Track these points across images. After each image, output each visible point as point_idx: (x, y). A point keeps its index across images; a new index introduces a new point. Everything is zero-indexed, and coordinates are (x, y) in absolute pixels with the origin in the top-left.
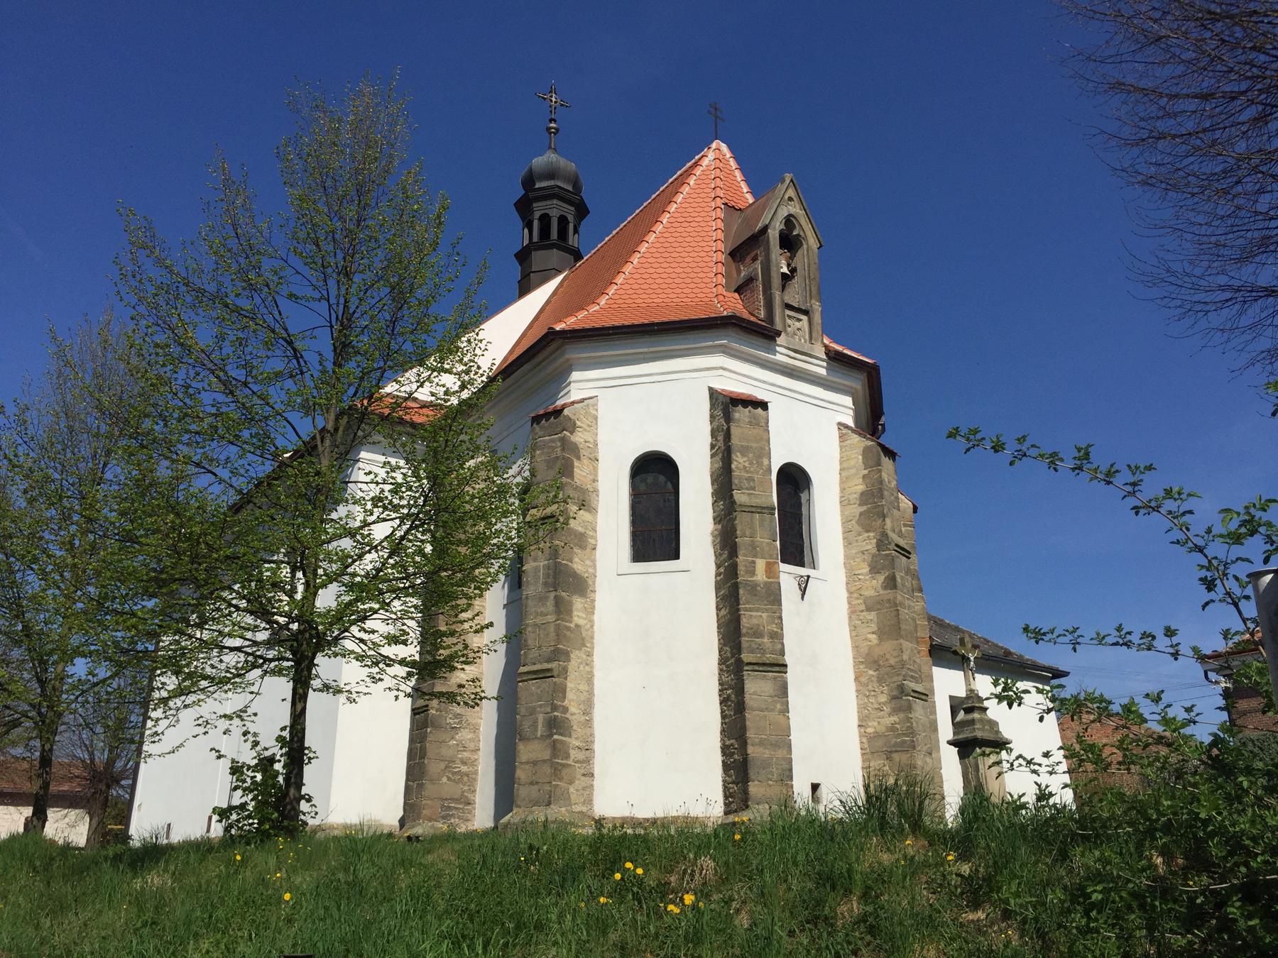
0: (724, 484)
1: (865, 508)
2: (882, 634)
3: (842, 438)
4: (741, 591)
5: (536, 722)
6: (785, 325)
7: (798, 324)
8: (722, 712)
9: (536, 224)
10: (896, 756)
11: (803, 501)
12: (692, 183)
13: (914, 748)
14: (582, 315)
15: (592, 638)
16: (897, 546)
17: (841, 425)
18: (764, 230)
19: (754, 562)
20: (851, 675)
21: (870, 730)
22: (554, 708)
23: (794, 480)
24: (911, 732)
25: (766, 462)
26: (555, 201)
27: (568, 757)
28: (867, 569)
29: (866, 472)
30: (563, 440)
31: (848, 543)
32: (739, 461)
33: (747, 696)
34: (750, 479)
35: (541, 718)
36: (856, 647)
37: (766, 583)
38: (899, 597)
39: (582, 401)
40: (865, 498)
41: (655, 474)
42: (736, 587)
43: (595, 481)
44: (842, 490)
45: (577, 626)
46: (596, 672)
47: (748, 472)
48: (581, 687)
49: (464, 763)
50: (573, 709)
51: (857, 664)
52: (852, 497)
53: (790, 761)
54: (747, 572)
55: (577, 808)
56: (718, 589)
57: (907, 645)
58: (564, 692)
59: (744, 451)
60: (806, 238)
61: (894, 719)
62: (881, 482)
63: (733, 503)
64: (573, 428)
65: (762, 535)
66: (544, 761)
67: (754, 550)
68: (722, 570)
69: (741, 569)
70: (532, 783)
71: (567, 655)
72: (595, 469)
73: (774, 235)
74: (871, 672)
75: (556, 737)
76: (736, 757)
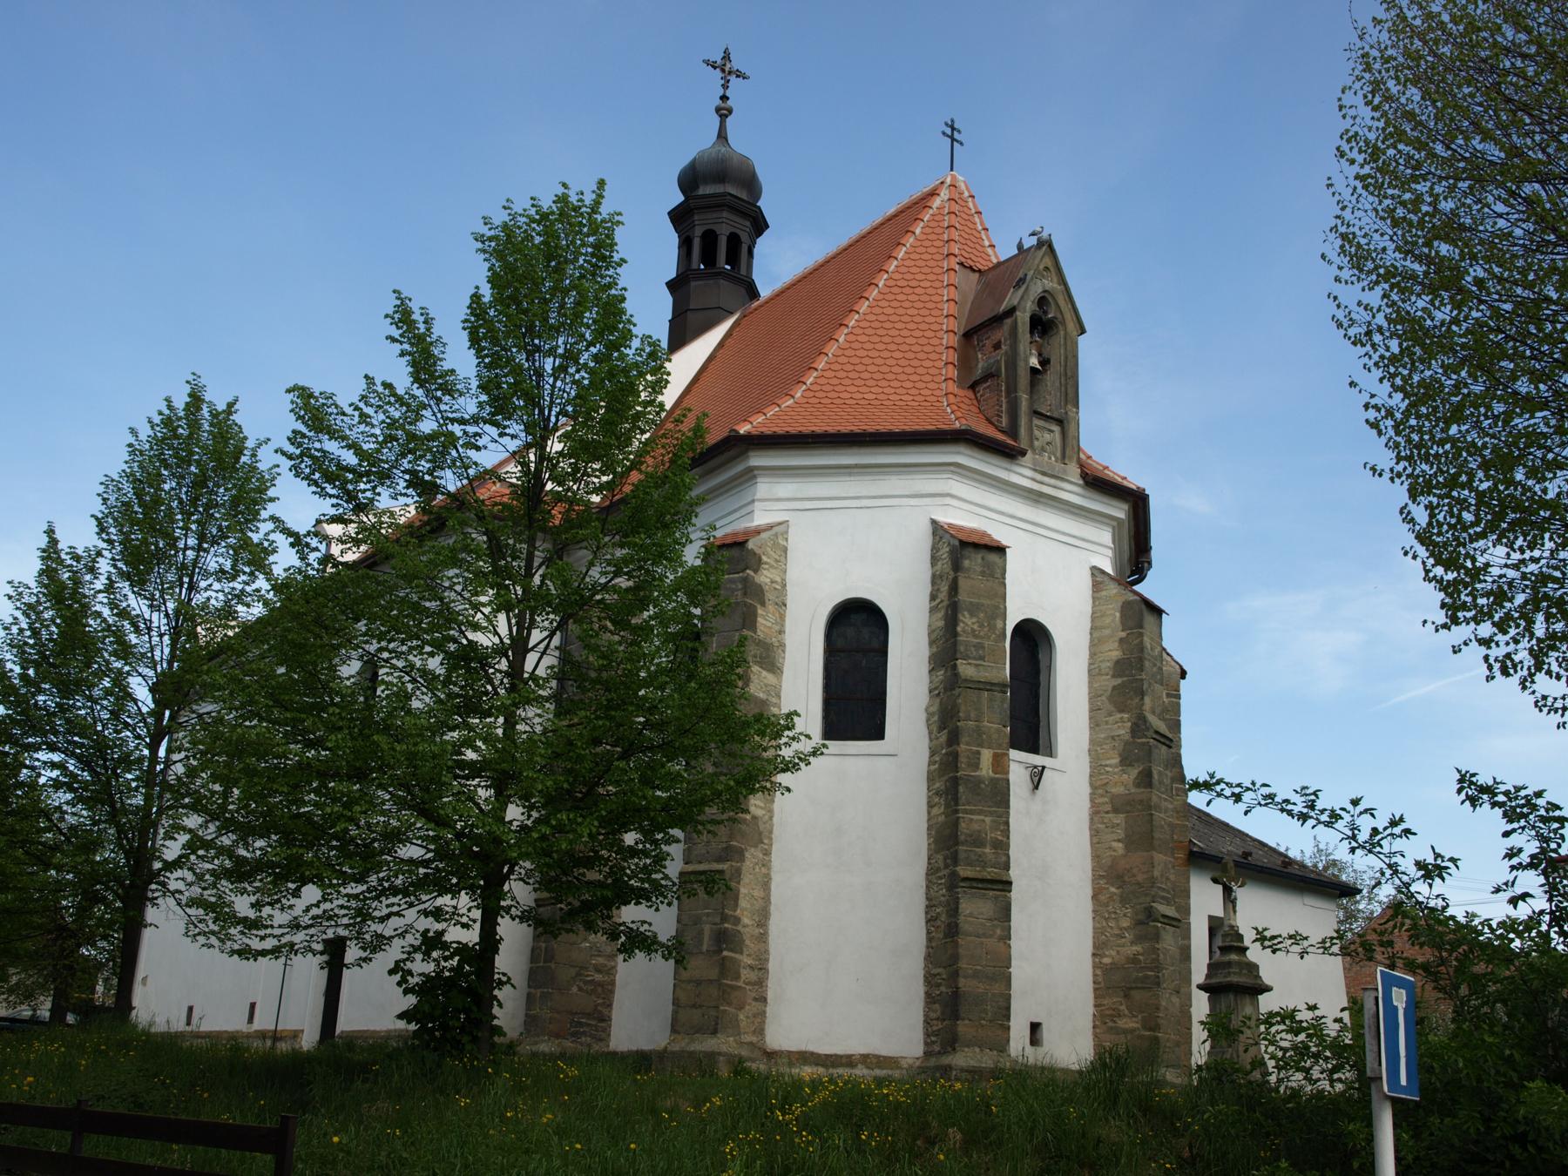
0: (946, 651)
1: (1119, 681)
2: (1130, 842)
3: (1097, 587)
4: (961, 789)
5: (701, 932)
6: (1032, 438)
7: (1047, 437)
8: (928, 932)
9: (697, 243)
10: (1137, 995)
11: (1043, 665)
12: (918, 231)
13: (1158, 984)
14: (772, 411)
15: (771, 832)
16: (1157, 732)
17: (1096, 572)
18: (1011, 312)
19: (979, 753)
20: (1088, 891)
21: (1106, 960)
22: (725, 918)
23: (1032, 637)
24: (1157, 966)
25: (999, 624)
26: (725, 214)
27: (738, 977)
28: (1116, 761)
29: (1123, 634)
30: (745, 580)
31: (1095, 724)
32: (967, 622)
33: (962, 918)
34: (980, 646)
35: (707, 928)
36: (1096, 857)
37: (992, 779)
38: (1155, 799)
39: (770, 527)
40: (1120, 667)
41: (857, 629)
42: (955, 782)
43: (781, 632)
44: (1092, 655)
45: (754, 818)
46: (773, 875)
47: (976, 636)
48: (756, 893)
49: (598, 971)
50: (746, 921)
51: (1096, 878)
52: (1104, 665)
53: (1008, 998)
54: (969, 765)
55: (748, 1038)
56: (931, 779)
57: (1159, 858)
58: (736, 899)
59: (974, 609)
60: (1064, 323)
61: (1137, 948)
62: (1141, 649)
63: (956, 675)
64: (756, 563)
65: (993, 717)
66: (711, 981)
67: (980, 739)
68: (937, 758)
69: (963, 759)
70: (694, 1006)
71: (740, 855)
72: (782, 617)
73: (1023, 317)
74: (1113, 889)
75: (725, 953)
76: (943, 989)
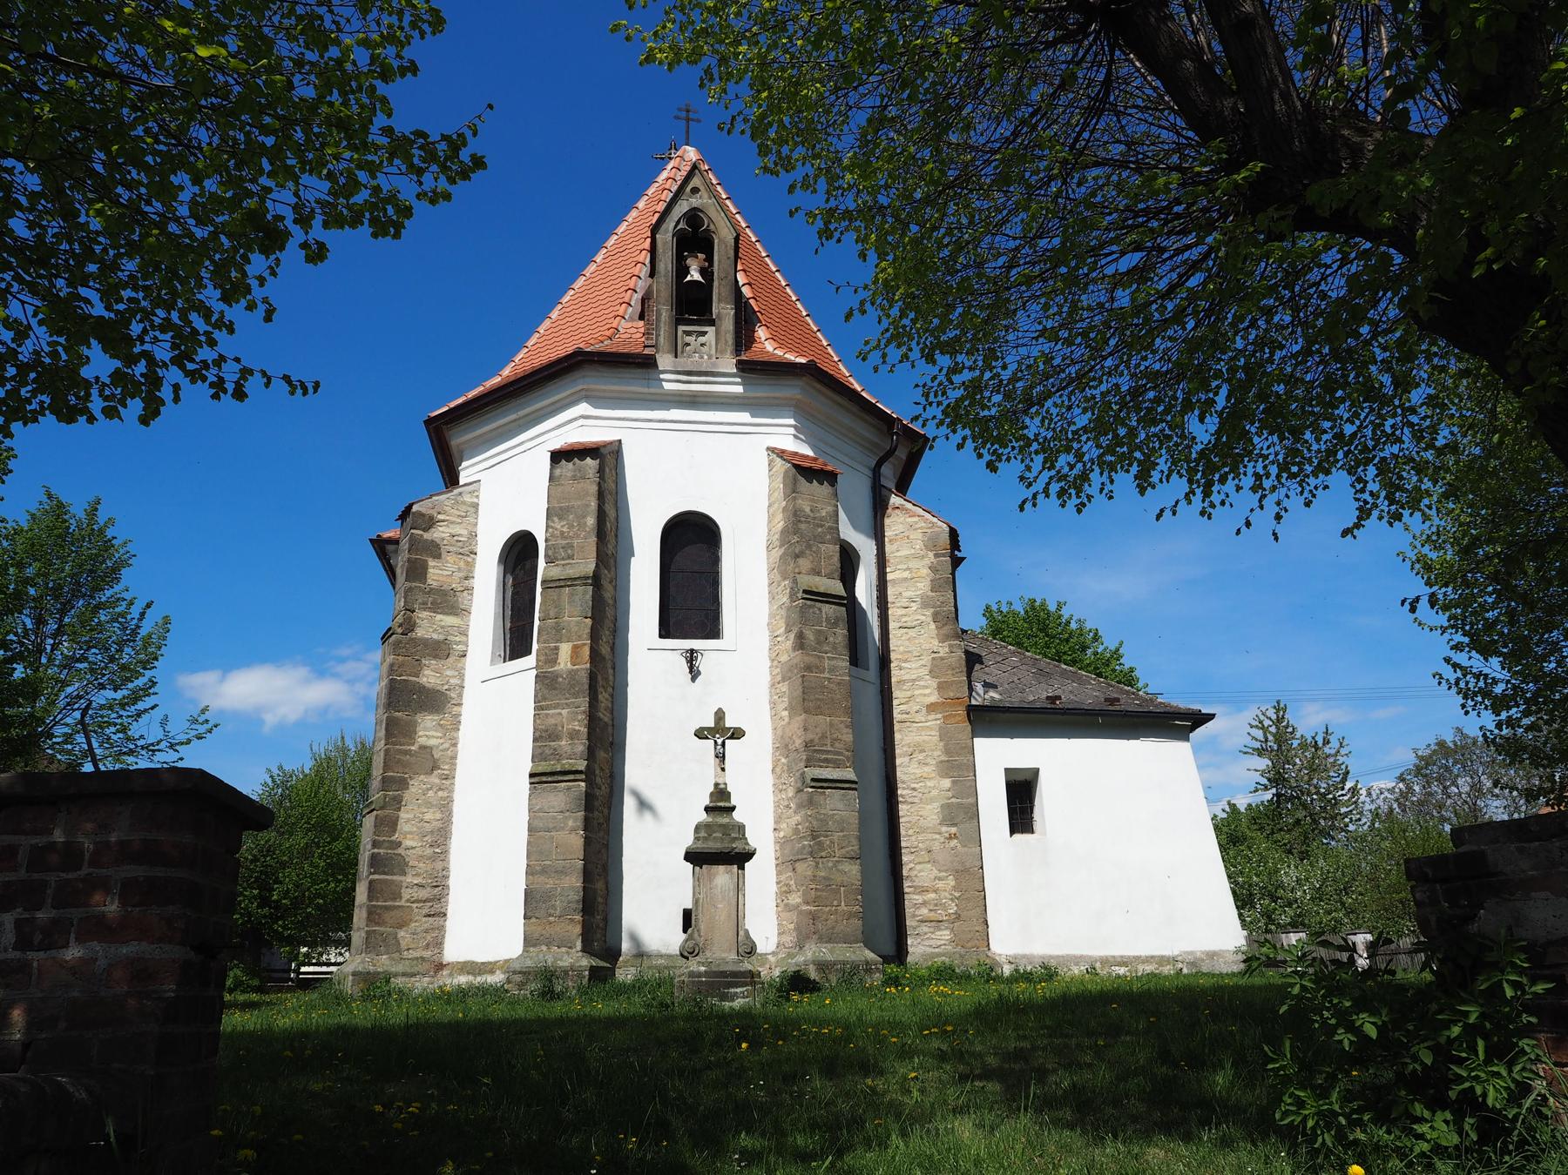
19: (557, 648)
